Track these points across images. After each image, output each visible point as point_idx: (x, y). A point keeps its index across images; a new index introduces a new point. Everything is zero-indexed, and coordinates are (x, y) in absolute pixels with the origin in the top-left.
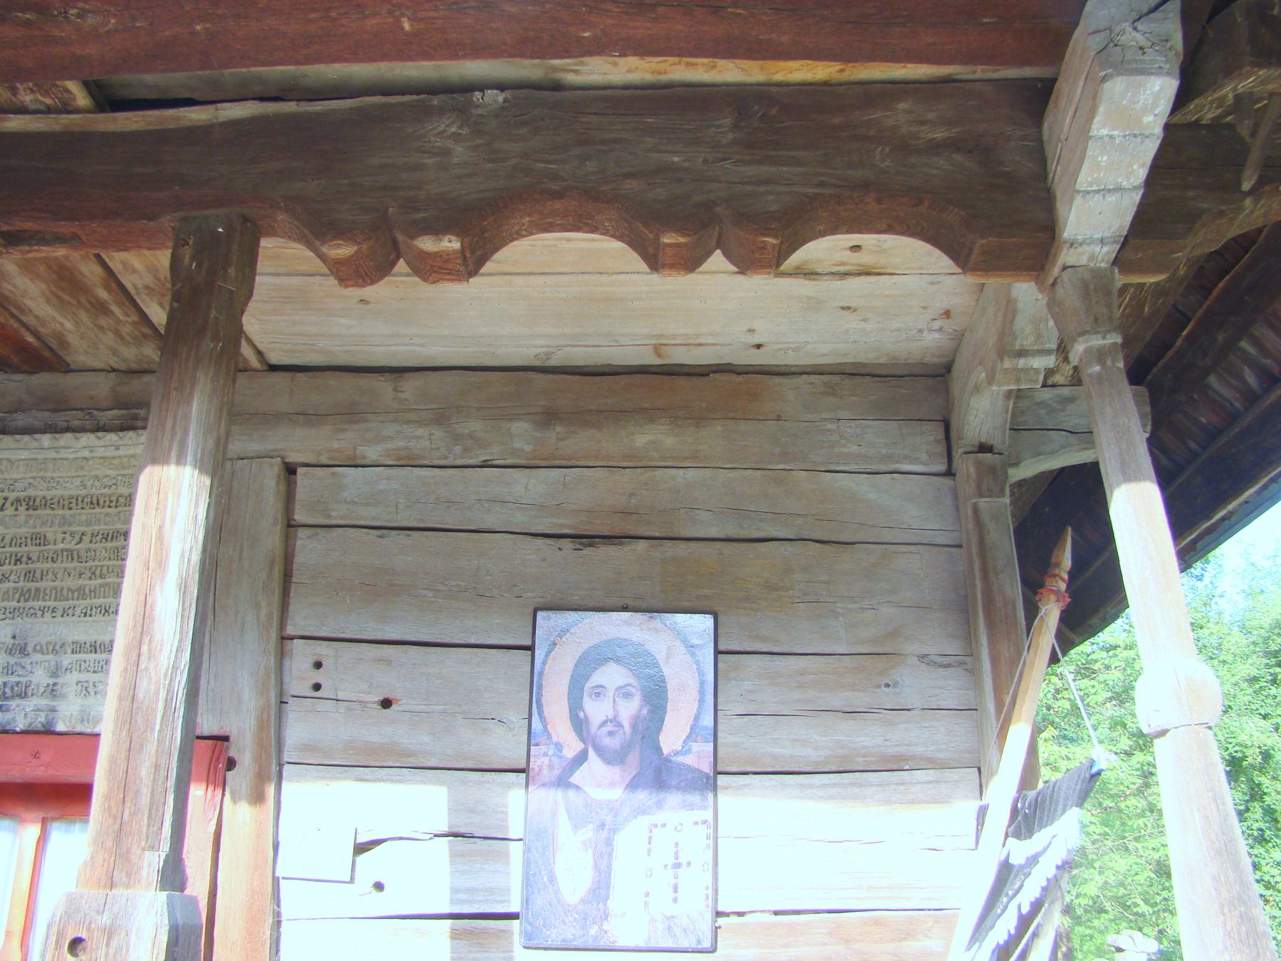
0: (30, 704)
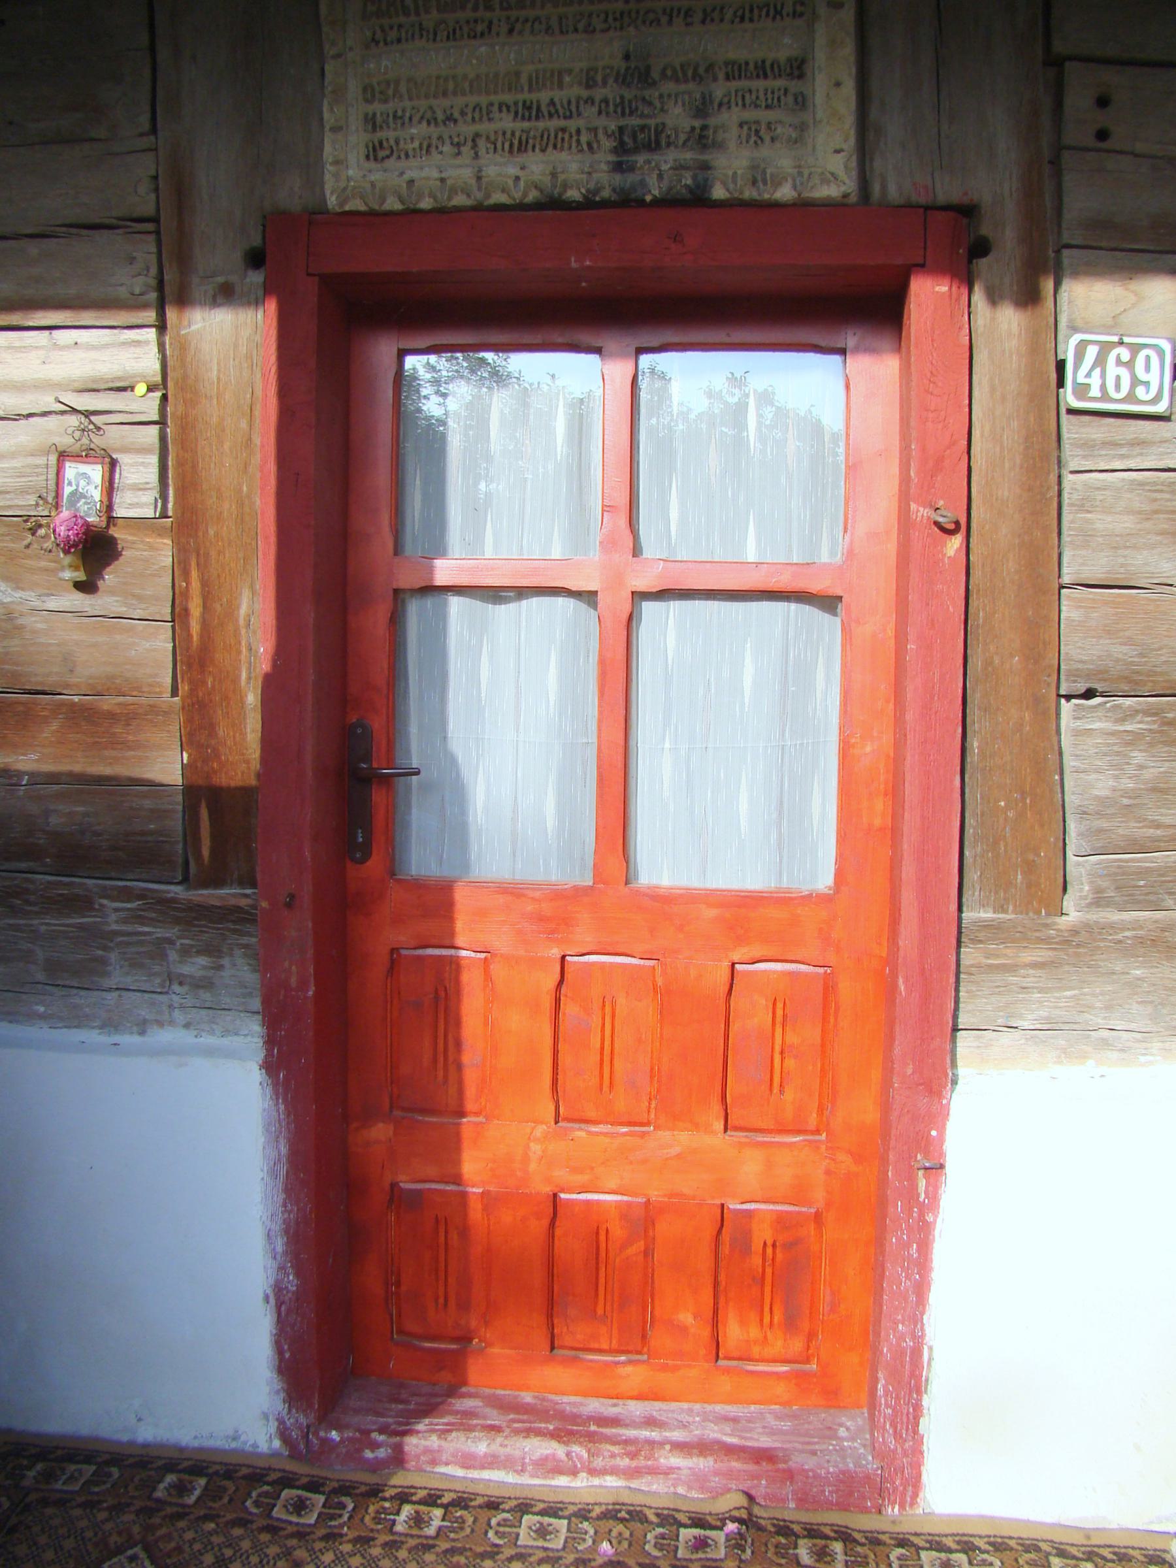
0: (668, 159)
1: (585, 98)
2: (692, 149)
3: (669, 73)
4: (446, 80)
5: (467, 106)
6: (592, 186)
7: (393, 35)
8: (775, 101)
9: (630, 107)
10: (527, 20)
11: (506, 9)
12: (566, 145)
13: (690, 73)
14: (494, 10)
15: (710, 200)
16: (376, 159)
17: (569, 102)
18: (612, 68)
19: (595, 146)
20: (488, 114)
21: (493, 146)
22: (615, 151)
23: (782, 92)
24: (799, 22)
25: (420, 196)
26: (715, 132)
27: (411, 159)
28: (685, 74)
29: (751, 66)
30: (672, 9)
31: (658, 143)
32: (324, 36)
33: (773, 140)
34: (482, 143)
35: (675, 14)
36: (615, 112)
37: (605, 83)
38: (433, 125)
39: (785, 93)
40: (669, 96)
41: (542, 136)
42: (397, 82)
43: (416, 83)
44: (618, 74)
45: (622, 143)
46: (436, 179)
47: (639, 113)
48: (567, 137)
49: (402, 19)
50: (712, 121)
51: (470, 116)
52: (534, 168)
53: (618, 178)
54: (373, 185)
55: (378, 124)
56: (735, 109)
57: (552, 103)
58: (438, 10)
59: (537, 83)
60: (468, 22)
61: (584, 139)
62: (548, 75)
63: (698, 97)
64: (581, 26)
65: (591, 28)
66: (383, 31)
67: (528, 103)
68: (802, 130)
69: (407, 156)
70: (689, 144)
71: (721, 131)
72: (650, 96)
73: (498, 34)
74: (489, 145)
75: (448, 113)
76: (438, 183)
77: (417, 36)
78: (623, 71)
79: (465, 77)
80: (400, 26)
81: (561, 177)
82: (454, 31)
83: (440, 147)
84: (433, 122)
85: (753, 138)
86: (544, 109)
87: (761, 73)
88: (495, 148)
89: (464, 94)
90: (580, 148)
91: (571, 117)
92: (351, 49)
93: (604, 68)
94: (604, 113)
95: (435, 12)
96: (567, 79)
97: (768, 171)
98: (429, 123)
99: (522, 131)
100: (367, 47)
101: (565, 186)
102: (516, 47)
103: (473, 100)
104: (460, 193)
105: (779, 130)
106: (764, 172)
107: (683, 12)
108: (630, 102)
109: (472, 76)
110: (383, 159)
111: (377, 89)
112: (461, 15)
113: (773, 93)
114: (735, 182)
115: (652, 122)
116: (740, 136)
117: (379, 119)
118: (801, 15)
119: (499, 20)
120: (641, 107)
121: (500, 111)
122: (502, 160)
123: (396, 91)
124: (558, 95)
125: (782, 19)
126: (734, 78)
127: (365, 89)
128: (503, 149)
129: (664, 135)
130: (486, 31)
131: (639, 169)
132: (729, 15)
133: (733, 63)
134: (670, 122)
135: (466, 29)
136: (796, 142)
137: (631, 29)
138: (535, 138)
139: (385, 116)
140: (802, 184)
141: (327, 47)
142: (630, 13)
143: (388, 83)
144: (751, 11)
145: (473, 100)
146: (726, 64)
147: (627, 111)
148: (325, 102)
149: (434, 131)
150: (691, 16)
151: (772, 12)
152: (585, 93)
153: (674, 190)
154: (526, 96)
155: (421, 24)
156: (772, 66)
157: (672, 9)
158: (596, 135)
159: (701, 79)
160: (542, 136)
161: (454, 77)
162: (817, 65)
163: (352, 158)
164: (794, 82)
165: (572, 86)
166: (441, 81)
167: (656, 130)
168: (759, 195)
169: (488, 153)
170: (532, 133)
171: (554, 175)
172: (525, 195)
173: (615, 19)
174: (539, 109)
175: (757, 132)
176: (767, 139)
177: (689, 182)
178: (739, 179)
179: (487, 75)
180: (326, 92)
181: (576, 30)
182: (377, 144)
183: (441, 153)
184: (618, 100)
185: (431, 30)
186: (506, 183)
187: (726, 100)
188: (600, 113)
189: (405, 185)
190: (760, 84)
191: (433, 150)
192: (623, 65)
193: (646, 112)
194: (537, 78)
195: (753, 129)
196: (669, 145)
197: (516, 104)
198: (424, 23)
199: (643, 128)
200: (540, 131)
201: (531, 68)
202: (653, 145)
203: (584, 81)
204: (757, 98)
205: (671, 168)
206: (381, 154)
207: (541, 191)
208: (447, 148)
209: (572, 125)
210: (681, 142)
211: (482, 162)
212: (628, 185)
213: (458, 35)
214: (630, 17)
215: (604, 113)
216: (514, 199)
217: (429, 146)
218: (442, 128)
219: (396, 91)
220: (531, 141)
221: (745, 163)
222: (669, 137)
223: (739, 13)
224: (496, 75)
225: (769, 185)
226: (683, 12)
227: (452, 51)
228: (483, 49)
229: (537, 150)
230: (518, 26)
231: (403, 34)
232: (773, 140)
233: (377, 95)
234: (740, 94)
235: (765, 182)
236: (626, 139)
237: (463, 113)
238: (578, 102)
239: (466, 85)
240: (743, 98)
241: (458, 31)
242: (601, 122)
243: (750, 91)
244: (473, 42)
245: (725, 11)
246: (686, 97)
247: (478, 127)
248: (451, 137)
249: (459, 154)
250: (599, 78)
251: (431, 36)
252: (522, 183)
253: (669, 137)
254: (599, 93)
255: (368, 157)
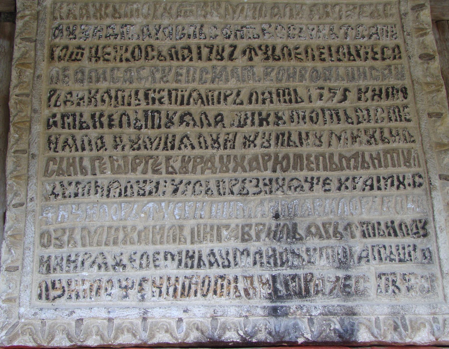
1: (241, 250)
2: (338, 296)
3: (313, 230)
4: (117, 229)
5: (135, 253)
6: (249, 329)
7: (71, 190)
8: (407, 255)
9: (282, 259)
10: (189, 183)
11: (171, 173)
12: (225, 290)
13: (331, 230)
14: (161, 173)
15: (355, 342)
16: (47, 298)
17: (228, 254)
18: (264, 225)
19: (251, 292)
20: (154, 261)
21: (158, 290)
22: (270, 297)
23: (411, 248)
24: (418, 191)
25: (88, 335)
26: (357, 282)
27: (82, 299)
28: (327, 232)
29: (383, 227)
30: (312, 178)
31: (307, 291)
32: (8, 187)
33: (408, 289)
34: (147, 287)
35: (315, 181)
36: (269, 263)
37: (258, 238)
38: (103, 269)
39: (415, 250)
40: (315, 250)
41: (203, 282)
42: (72, 230)
43: (89, 232)
44: (269, 229)
45: (276, 290)
46: (105, 319)
47: (290, 264)
48: (225, 283)
49: (80, 177)
50: (353, 272)
51: (138, 262)
52: (196, 311)
53: (273, 323)
54: (43, 322)
55: (52, 266)
56: (372, 262)
57: (212, 253)
58: (112, 171)
59: (199, 235)
60: (138, 182)
61: (241, 286)
62: (208, 229)
63: (340, 251)
64: (236, 189)
65: (245, 191)
66: (62, 186)
67: (191, 254)
68: (432, 281)
69: (78, 296)
70: (335, 291)
71: (361, 280)
72: (298, 249)
73: (164, 193)
74: (154, 289)
75: (118, 259)
76: (106, 322)
77: (92, 191)
78: (273, 228)
79: (134, 228)
80: (78, 183)
81: (222, 320)
82: (126, 188)
83: (109, 289)
84: (103, 265)
85: (391, 288)
86: (204, 258)
87: (392, 231)
88: (161, 292)
89: (132, 243)
90: (237, 294)
91: (229, 266)
92: (32, 200)
93: (257, 225)
94: (258, 264)
95: (109, 172)
96: (225, 233)
97: (407, 317)
98: (100, 267)
99: (185, 277)
100: (47, 199)
101: (224, 328)
102: (180, 205)
103: (141, 248)
104: (126, 333)
105: (413, 281)
106: (403, 318)
107: (321, 180)
108: (281, 254)
109: (140, 227)
110: (55, 298)
111: (54, 235)
112: (132, 176)
113: (404, 248)
114: (378, 327)
115: (301, 272)
116: (379, 286)
117: (53, 263)
118: (420, 185)
119: (166, 182)
120: (291, 259)
121: (166, 259)
122: (166, 302)
123: (71, 237)
124: (217, 247)
125: (405, 188)
126: (370, 236)
127: (42, 235)
128: (167, 293)
129: (312, 284)
130: (154, 190)
131: (292, 314)
132: (360, 185)
133: (368, 223)
134: (317, 274)
135: (136, 188)
136: (428, 291)
137: (279, 192)
138: (196, 284)
139: (59, 259)
140: (439, 330)
141: (10, 196)
142: (277, 179)
143: (64, 230)
144: (379, 181)
145: (141, 248)
146: (362, 224)
147: (279, 261)
148: (4, 245)
149: (104, 275)
150: (329, 184)
151: (396, 183)
152: (241, 246)
153: (324, 334)
154: (190, 247)
155: (96, 182)
156: (400, 225)
157: (312, 178)
158: (252, 283)
159: (342, 237)
160: (203, 282)
161: (124, 227)
162: (437, 226)
163: (25, 298)
164: (420, 240)
165: (229, 239)
166: (113, 231)
167: (305, 278)
168: (401, 338)
169: (153, 296)
170: (194, 280)
171: (214, 318)
172: (187, 335)
173: (265, 185)
174: (200, 258)
175: (394, 282)
176: (403, 288)
177: (338, 327)
178: (382, 325)
179: (154, 227)
180: (6, 235)
181: (232, 193)
182: (50, 285)
183: (110, 295)
184: (271, 253)
185: (105, 188)
186: (170, 324)
187: (364, 254)
188: (255, 263)
189: (74, 323)
190: (392, 241)
191: (102, 291)
192: (274, 223)
193: (296, 263)
194: (199, 231)
195: (390, 280)
196: (317, 292)
197: (180, 253)
198: (99, 181)
199: (294, 278)
200: (202, 277)
201: (192, 222)
202: (303, 293)
203: (240, 235)
204: (391, 253)
205: (320, 314)
206: (53, 293)
207: (202, 333)
208: (116, 291)
209: (231, 273)
210: (327, 291)
211: (147, 304)
212: (282, 329)
213: (129, 193)
214: (277, 183)
215: (258, 264)
216: (177, 339)
217: (99, 288)
218: (111, 272)
219: (71, 237)
220: (193, 286)
221: (386, 310)
222: (317, 285)
223: (369, 183)
224: (162, 228)
225: (410, 330)
226: (321, 180)
227: (123, 205)
228: (151, 205)
229: (199, 294)
230: (182, 188)
231: (80, 190)
232: (408, 289)
233: (53, 241)
234: (376, 249)
235: (406, 329)
236: (278, 286)
237: (131, 260)
238: (235, 254)
239: (135, 236)
240: (379, 252)
241: (129, 189)
242: (256, 271)
243: (384, 247)
244: (142, 198)
245: (356, 180)
246: (330, 251)
247: (144, 273)
248: (119, 281)
249: (126, 296)
250: (253, 233)
251: (105, 193)
252: (184, 325)
253: (317, 285)
254: (253, 247)
255: (40, 296)
